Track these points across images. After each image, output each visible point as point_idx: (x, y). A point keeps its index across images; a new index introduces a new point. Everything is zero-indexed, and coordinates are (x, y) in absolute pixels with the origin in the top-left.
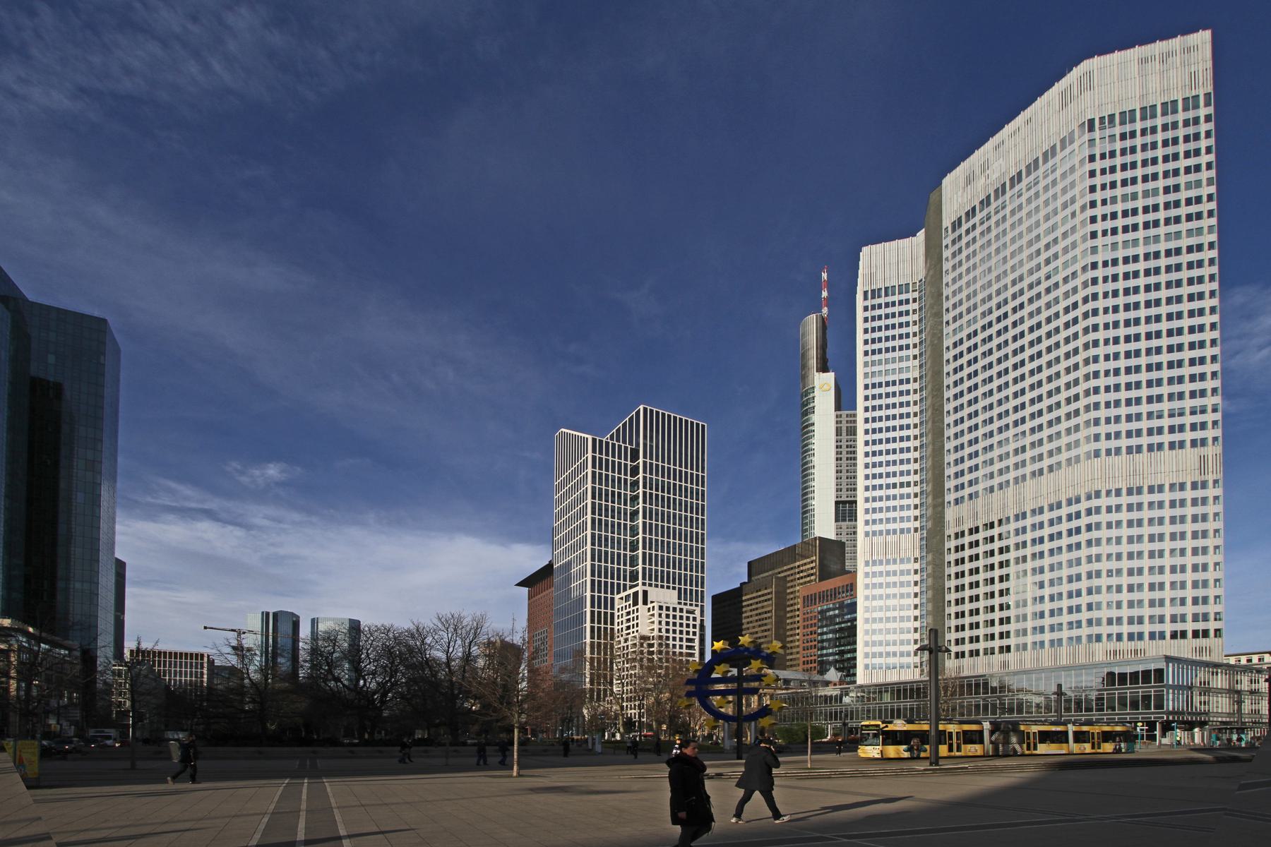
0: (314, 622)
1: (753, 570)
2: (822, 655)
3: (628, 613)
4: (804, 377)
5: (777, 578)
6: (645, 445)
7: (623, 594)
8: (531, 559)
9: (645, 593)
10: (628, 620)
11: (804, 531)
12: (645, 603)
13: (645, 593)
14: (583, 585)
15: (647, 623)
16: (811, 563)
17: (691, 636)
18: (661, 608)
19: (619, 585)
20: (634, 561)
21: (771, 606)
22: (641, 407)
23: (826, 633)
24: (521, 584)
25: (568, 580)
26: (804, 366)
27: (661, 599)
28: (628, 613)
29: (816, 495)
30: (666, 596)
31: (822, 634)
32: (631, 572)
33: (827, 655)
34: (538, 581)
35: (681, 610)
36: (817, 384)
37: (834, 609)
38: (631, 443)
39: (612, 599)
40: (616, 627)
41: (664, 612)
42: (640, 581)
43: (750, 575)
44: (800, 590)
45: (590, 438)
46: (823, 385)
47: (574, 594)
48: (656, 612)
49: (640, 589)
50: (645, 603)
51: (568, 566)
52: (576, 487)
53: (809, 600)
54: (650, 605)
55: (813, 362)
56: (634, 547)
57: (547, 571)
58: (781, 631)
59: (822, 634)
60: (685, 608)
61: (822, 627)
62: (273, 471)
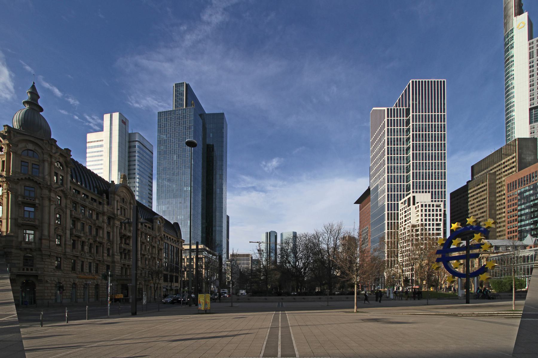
0: (282, 235)
1: (475, 171)
2: (521, 226)
3: (405, 212)
4: (506, 16)
5: (490, 174)
6: (413, 104)
7: (403, 200)
8: (361, 186)
9: (414, 197)
10: (405, 216)
11: (507, 136)
12: (414, 204)
13: (414, 197)
14: (383, 199)
15: (415, 217)
16: (512, 159)
17: (439, 222)
18: (422, 206)
19: (404, 194)
20: (408, 177)
21: (486, 195)
22: (411, 82)
23: (524, 209)
24: (356, 203)
25: (377, 197)
26: (506, 9)
27: (422, 200)
28: (405, 212)
29: (515, 108)
30: (424, 198)
31: (521, 210)
32: (407, 186)
33: (525, 225)
34: (364, 199)
35: (433, 206)
36: (515, 26)
37: (529, 190)
38: (406, 106)
39: (398, 204)
40: (399, 221)
41: (424, 208)
42: (411, 191)
43: (473, 175)
44: (506, 180)
45: (386, 109)
46: (520, 24)
47: (380, 204)
48: (420, 209)
49: (411, 195)
50: (414, 204)
51: (377, 188)
52: (380, 140)
53: (512, 186)
54: (416, 205)
55: (512, 11)
56: (408, 171)
57: (367, 193)
58: (493, 212)
59: (521, 210)
60: (435, 204)
61: (521, 205)
62: (275, 162)
